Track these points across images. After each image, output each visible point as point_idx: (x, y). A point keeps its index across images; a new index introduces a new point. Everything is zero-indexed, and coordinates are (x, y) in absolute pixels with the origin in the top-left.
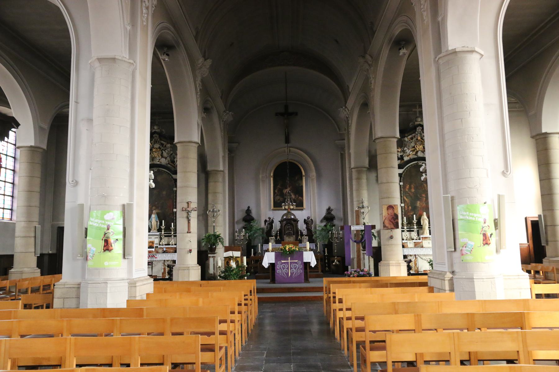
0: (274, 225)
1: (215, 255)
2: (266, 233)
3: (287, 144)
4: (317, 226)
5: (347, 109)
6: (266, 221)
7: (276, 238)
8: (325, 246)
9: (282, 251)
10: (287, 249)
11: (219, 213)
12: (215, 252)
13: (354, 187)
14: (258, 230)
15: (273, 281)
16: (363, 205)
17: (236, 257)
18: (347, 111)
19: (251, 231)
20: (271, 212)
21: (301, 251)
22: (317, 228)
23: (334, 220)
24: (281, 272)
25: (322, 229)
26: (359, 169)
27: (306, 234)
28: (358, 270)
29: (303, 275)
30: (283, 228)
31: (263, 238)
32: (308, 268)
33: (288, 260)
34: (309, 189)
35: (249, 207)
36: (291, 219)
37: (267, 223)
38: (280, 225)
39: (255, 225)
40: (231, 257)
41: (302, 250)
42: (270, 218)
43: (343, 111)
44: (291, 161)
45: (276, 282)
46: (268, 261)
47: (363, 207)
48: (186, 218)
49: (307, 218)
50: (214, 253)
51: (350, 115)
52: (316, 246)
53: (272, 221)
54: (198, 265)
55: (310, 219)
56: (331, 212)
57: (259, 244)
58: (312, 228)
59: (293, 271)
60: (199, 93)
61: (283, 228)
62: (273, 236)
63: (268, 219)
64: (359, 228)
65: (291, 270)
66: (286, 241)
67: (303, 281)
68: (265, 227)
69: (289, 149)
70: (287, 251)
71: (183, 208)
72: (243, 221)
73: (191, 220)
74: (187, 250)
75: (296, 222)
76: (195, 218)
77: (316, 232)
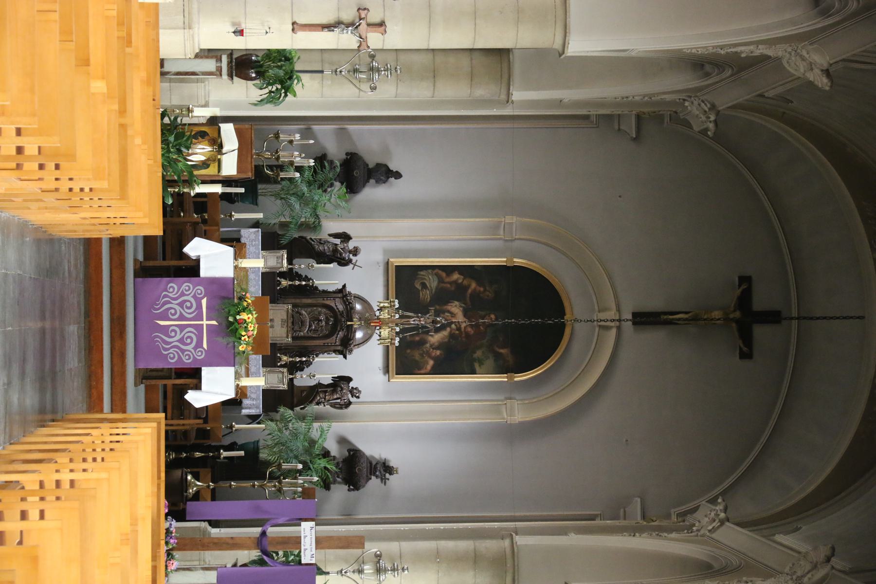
0: (330, 268)
1: (225, 76)
2: (305, 238)
3: (630, 317)
4: (325, 425)
5: (718, 527)
6: (345, 237)
7: (283, 275)
8: (252, 450)
9: (236, 301)
10: (244, 316)
11: (366, 87)
12: (235, 78)
13: (450, 545)
14: (315, 209)
15: (144, 272)
16: (386, 570)
17: (219, 161)
18: (710, 528)
19: (309, 184)
20: (380, 257)
21: (237, 359)
22: (316, 425)
23: (346, 487)
24: (170, 295)
25: (312, 443)
26: (509, 563)
27: (297, 383)
28: (172, 541)
29: (160, 365)
30: (320, 301)
31: (284, 225)
32: (179, 381)
33: (207, 320)
34: (459, 398)
35: (398, 175)
36: (351, 330)
37: (338, 241)
38: (331, 289)
39: (332, 200)
40: (221, 146)
41: (241, 365)
42: (355, 252)
43: (713, 514)
44: (568, 331)
45: (140, 280)
46: (206, 256)
47: (379, 571)
48: (336, 20)
49: (356, 389)
50: (231, 76)
51: (697, 535)
52: (254, 418)
53: (344, 259)
54: (197, 51)
55: (353, 400)
56: (377, 477)
57: (260, 216)
58: (318, 404)
59: (173, 334)
60: (722, 52)
61: (320, 301)
62: (290, 262)
63: (351, 245)
64: (308, 546)
65: (177, 329)
66: (271, 312)
67: (142, 366)
68: (324, 235)
69: (613, 324)
70: (238, 317)
71: (365, 9)
72: (347, 154)
73: (331, 33)
74: (242, 20)
75: (339, 348)
76: (338, 44)
77: (302, 418)
